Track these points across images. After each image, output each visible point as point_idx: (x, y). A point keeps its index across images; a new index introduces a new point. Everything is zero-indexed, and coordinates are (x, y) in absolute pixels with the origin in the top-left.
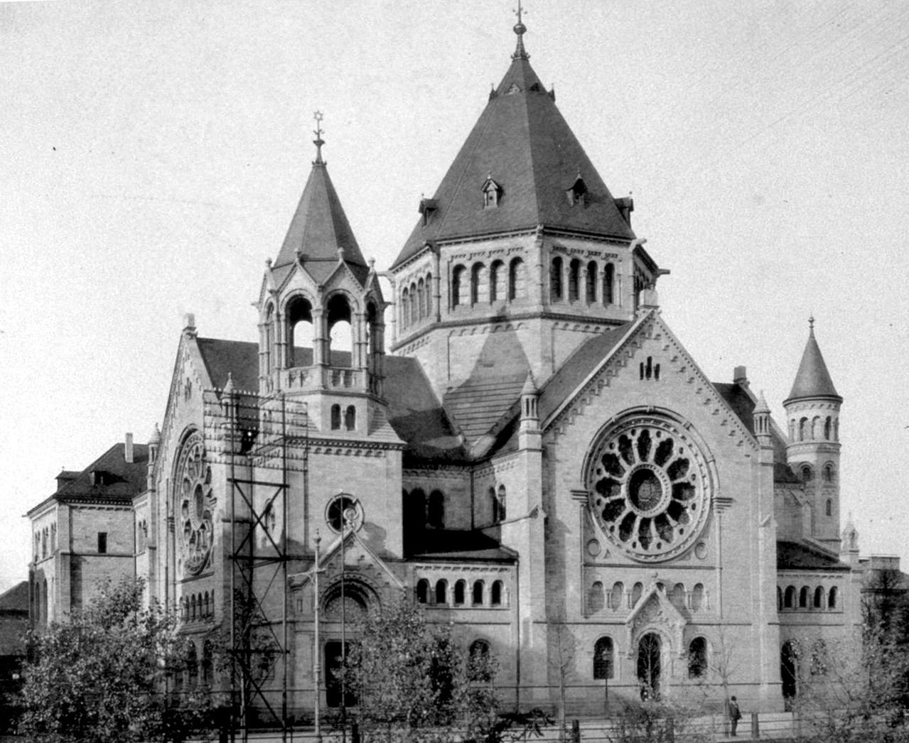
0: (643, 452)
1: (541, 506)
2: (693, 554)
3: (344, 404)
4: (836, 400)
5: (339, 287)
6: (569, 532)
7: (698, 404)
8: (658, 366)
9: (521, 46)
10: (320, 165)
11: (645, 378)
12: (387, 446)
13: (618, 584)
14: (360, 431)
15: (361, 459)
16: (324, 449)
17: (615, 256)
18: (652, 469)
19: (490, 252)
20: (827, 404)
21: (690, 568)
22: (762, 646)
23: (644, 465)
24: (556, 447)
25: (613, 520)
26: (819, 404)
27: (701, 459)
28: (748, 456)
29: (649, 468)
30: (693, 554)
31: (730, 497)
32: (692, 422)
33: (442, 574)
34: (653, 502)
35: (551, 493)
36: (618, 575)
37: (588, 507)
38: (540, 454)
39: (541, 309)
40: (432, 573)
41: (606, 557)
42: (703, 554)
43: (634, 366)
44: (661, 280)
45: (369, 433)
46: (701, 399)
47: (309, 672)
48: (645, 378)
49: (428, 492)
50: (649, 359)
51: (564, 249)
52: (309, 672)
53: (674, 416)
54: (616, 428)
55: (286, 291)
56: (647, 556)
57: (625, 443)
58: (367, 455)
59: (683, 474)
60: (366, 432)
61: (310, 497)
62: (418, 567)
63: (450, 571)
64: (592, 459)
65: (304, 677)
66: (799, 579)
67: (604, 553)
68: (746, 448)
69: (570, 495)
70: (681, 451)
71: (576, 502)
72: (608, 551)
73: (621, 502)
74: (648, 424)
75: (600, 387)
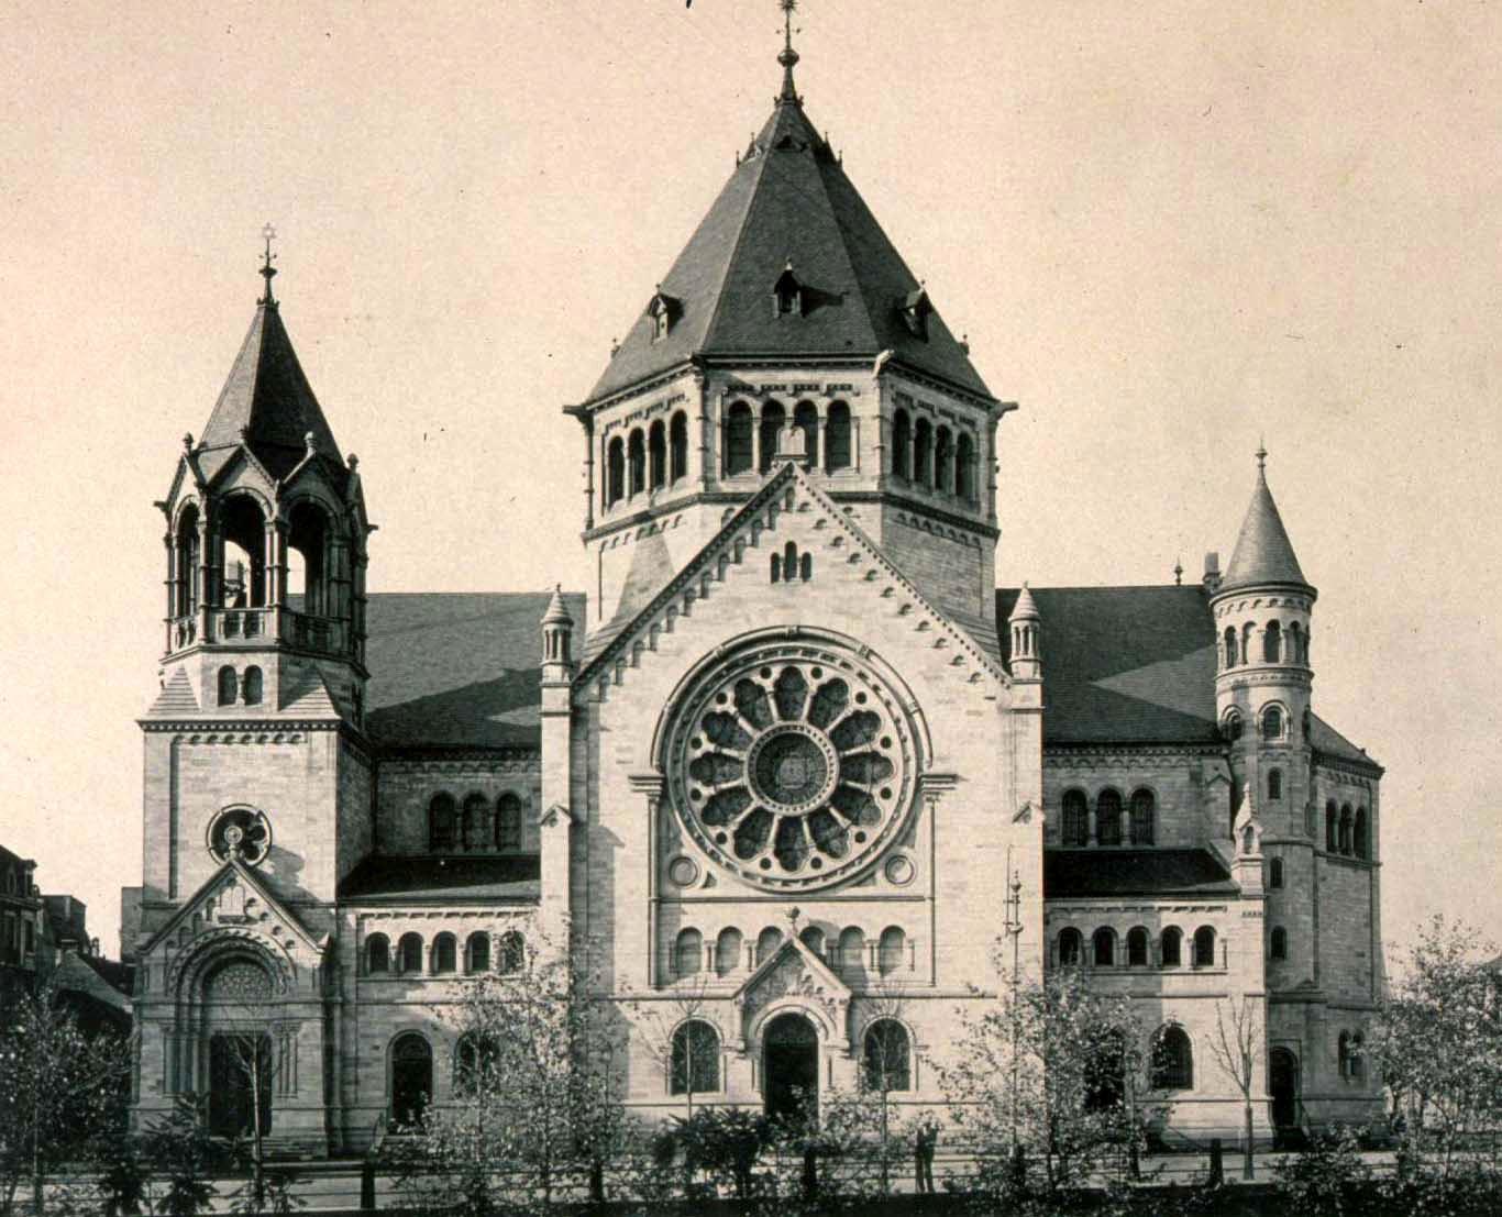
0: (786, 710)
1: (1038, 801)
2: (880, 875)
3: (241, 663)
5: (235, 485)
8: (807, 557)
9: (789, 82)
10: (269, 307)
11: (781, 579)
12: (307, 726)
14: (268, 708)
15: (269, 748)
17: (846, 388)
23: (788, 727)
24: (602, 706)
25: (724, 823)
26: (1237, 605)
27: (897, 711)
28: (992, 698)
29: (798, 731)
30: (880, 875)
31: (952, 771)
32: (872, 646)
33: (409, 925)
34: (808, 788)
35: (591, 784)
36: (726, 916)
37: (662, 801)
38: (567, 720)
39: (701, 488)
40: (392, 925)
41: (706, 886)
42: (902, 874)
45: (282, 705)
46: (892, 605)
47: (159, 1082)
48: (781, 579)
49: (459, 797)
50: (791, 547)
51: (748, 389)
52: (159, 1082)
53: (838, 638)
54: (732, 661)
55: (179, 501)
56: (825, 877)
57: (748, 696)
58: (276, 741)
59: (869, 738)
60: (275, 707)
62: (365, 916)
63: (457, 920)
64: (678, 722)
66: (1088, 917)
67: (701, 881)
68: (990, 684)
69: (627, 786)
70: (861, 698)
71: (638, 795)
75: (688, 601)
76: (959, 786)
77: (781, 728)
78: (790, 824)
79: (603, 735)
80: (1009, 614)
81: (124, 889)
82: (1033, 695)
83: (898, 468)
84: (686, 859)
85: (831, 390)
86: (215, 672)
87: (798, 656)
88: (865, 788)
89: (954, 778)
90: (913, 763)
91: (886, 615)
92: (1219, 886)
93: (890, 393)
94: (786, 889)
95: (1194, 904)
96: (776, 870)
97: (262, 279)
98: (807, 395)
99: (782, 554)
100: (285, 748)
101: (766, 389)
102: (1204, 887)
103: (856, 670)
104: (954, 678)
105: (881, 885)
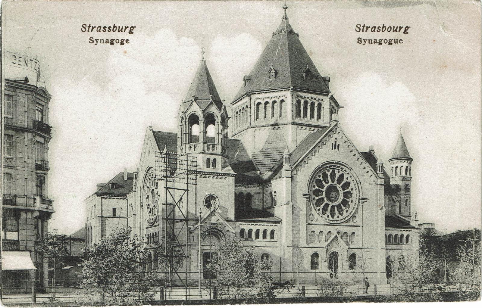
3: (212, 158)
8: (339, 145)
12: (228, 175)
14: (219, 169)
20: (406, 161)
27: (355, 181)
30: (351, 220)
36: (322, 228)
40: (247, 227)
43: (329, 144)
51: (301, 97)
53: (345, 164)
54: (321, 169)
55: (188, 112)
59: (348, 188)
62: (241, 224)
68: (374, 178)
73: (323, 199)
76: (368, 201)
77: (332, 184)
78: (333, 207)
79: (297, 183)
80: (376, 163)
81: (113, 209)
83: (298, 114)
84: (312, 214)
85: (319, 100)
87: (336, 168)
88: (348, 200)
90: (358, 195)
91: (355, 161)
92: (271, 219)
93: (295, 96)
94: (329, 222)
95: (409, 230)
96: (330, 218)
98: (314, 100)
99: (334, 144)
101: (305, 97)
102: (254, 219)
103: (347, 172)
104: (367, 176)
105: (351, 223)
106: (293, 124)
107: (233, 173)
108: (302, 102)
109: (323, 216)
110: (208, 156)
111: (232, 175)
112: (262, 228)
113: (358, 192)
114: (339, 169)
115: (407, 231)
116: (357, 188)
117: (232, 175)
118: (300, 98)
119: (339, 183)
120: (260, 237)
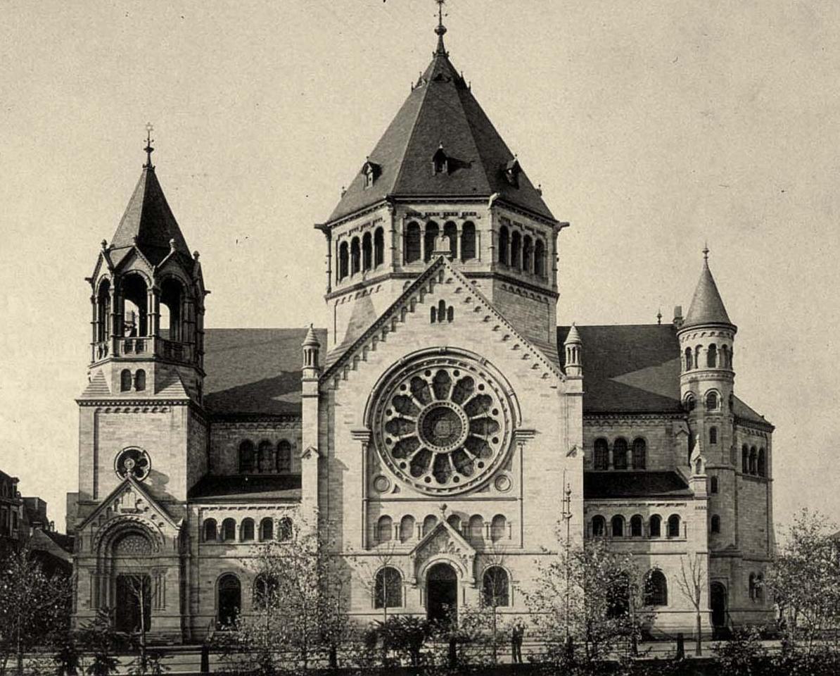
2: (492, 486)
3: (133, 368)
4: (728, 329)
6: (347, 469)
7: (496, 341)
8: (451, 308)
9: (441, 44)
10: (150, 169)
12: (171, 403)
13: (407, 518)
14: (149, 393)
16: (150, 408)
18: (450, 406)
19: (362, 227)
20: (709, 332)
21: (488, 499)
22: (141, 601)
29: (446, 406)
30: (492, 486)
32: (487, 358)
34: (452, 437)
36: (406, 508)
40: (218, 514)
41: (394, 492)
42: (504, 486)
43: (423, 310)
44: (563, 233)
45: (157, 392)
46: (499, 336)
50: (442, 303)
51: (418, 215)
52: (87, 601)
53: (468, 354)
54: (409, 366)
59: (486, 410)
61: (99, 451)
62: (203, 509)
63: (255, 511)
65: (84, 605)
66: (609, 509)
68: (554, 380)
69: (350, 436)
70: (481, 387)
72: (396, 486)
73: (414, 439)
74: (442, 364)
77: (436, 404)
78: (442, 457)
79: (337, 408)
82: (578, 386)
83: (502, 259)
86: (119, 373)
89: (534, 432)
90: (510, 423)
92: (683, 492)
94: (439, 494)
95: (668, 502)
97: (146, 154)
98: (451, 218)
100: (158, 415)
101: (428, 215)
102: (673, 492)
104: (534, 376)
105: (492, 492)
106: (496, 276)
107: (185, 397)
108: (422, 224)
109: (412, 478)
110: (126, 365)
111: (182, 402)
112: (257, 516)
113: (509, 417)
114: (457, 365)
115: (668, 505)
116: (509, 409)
117: (182, 402)
118: (414, 219)
119: (457, 398)
120: (680, 534)
